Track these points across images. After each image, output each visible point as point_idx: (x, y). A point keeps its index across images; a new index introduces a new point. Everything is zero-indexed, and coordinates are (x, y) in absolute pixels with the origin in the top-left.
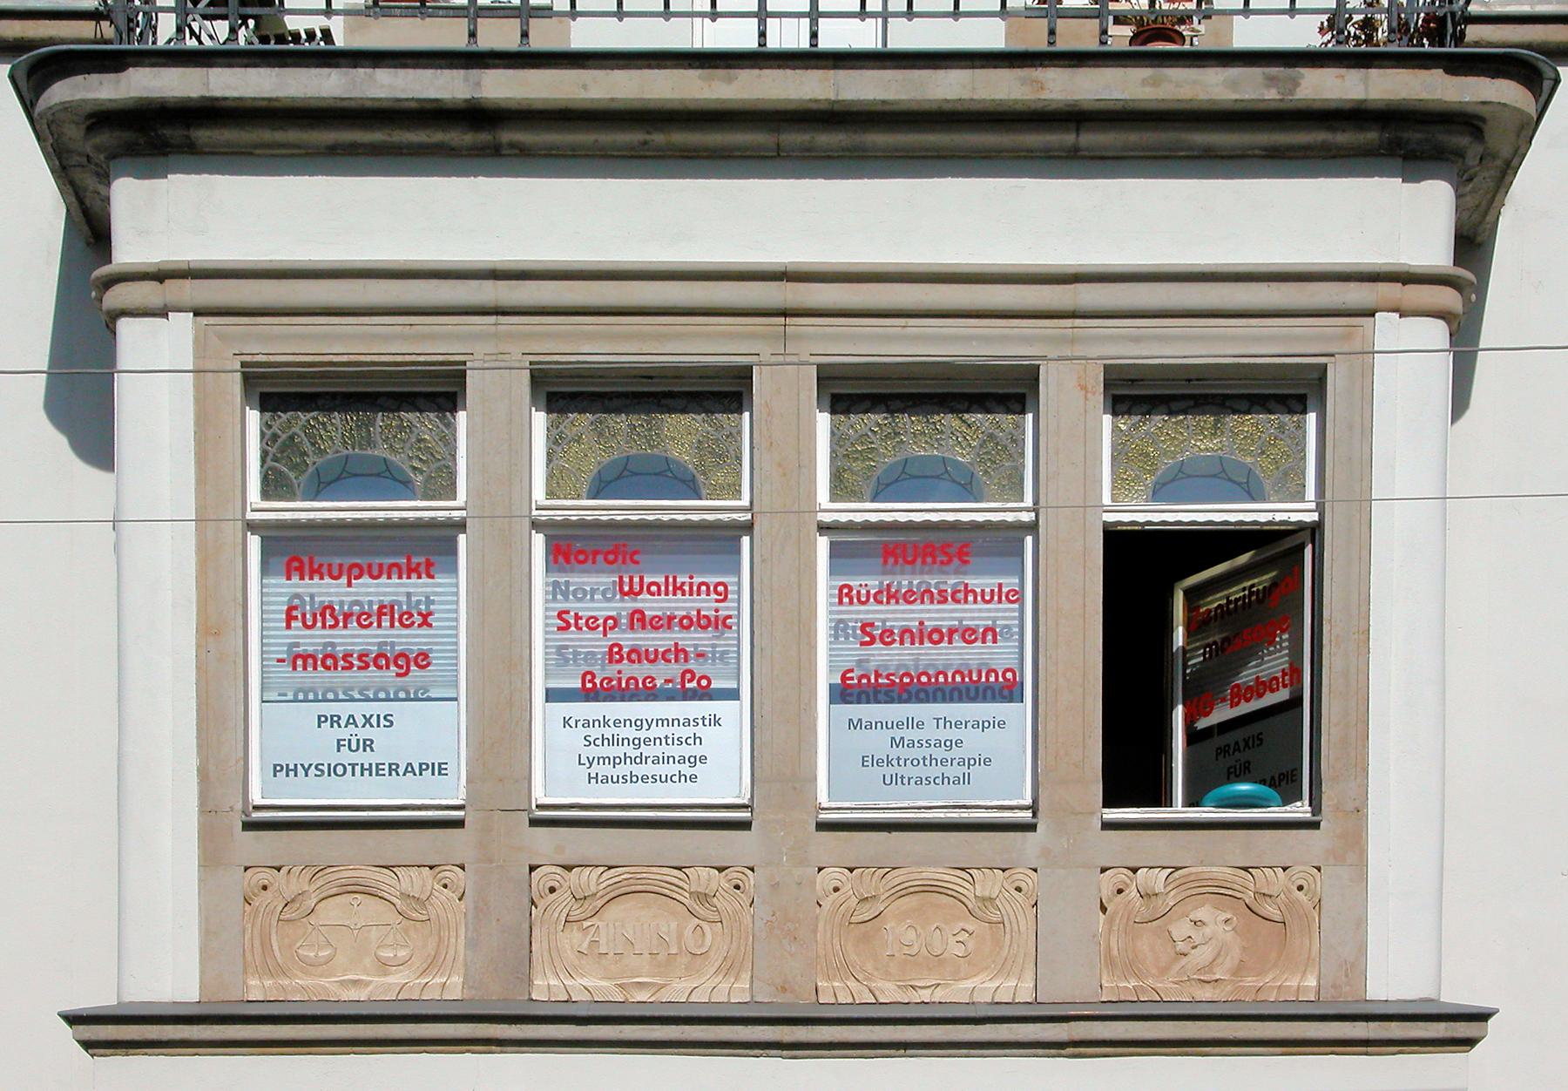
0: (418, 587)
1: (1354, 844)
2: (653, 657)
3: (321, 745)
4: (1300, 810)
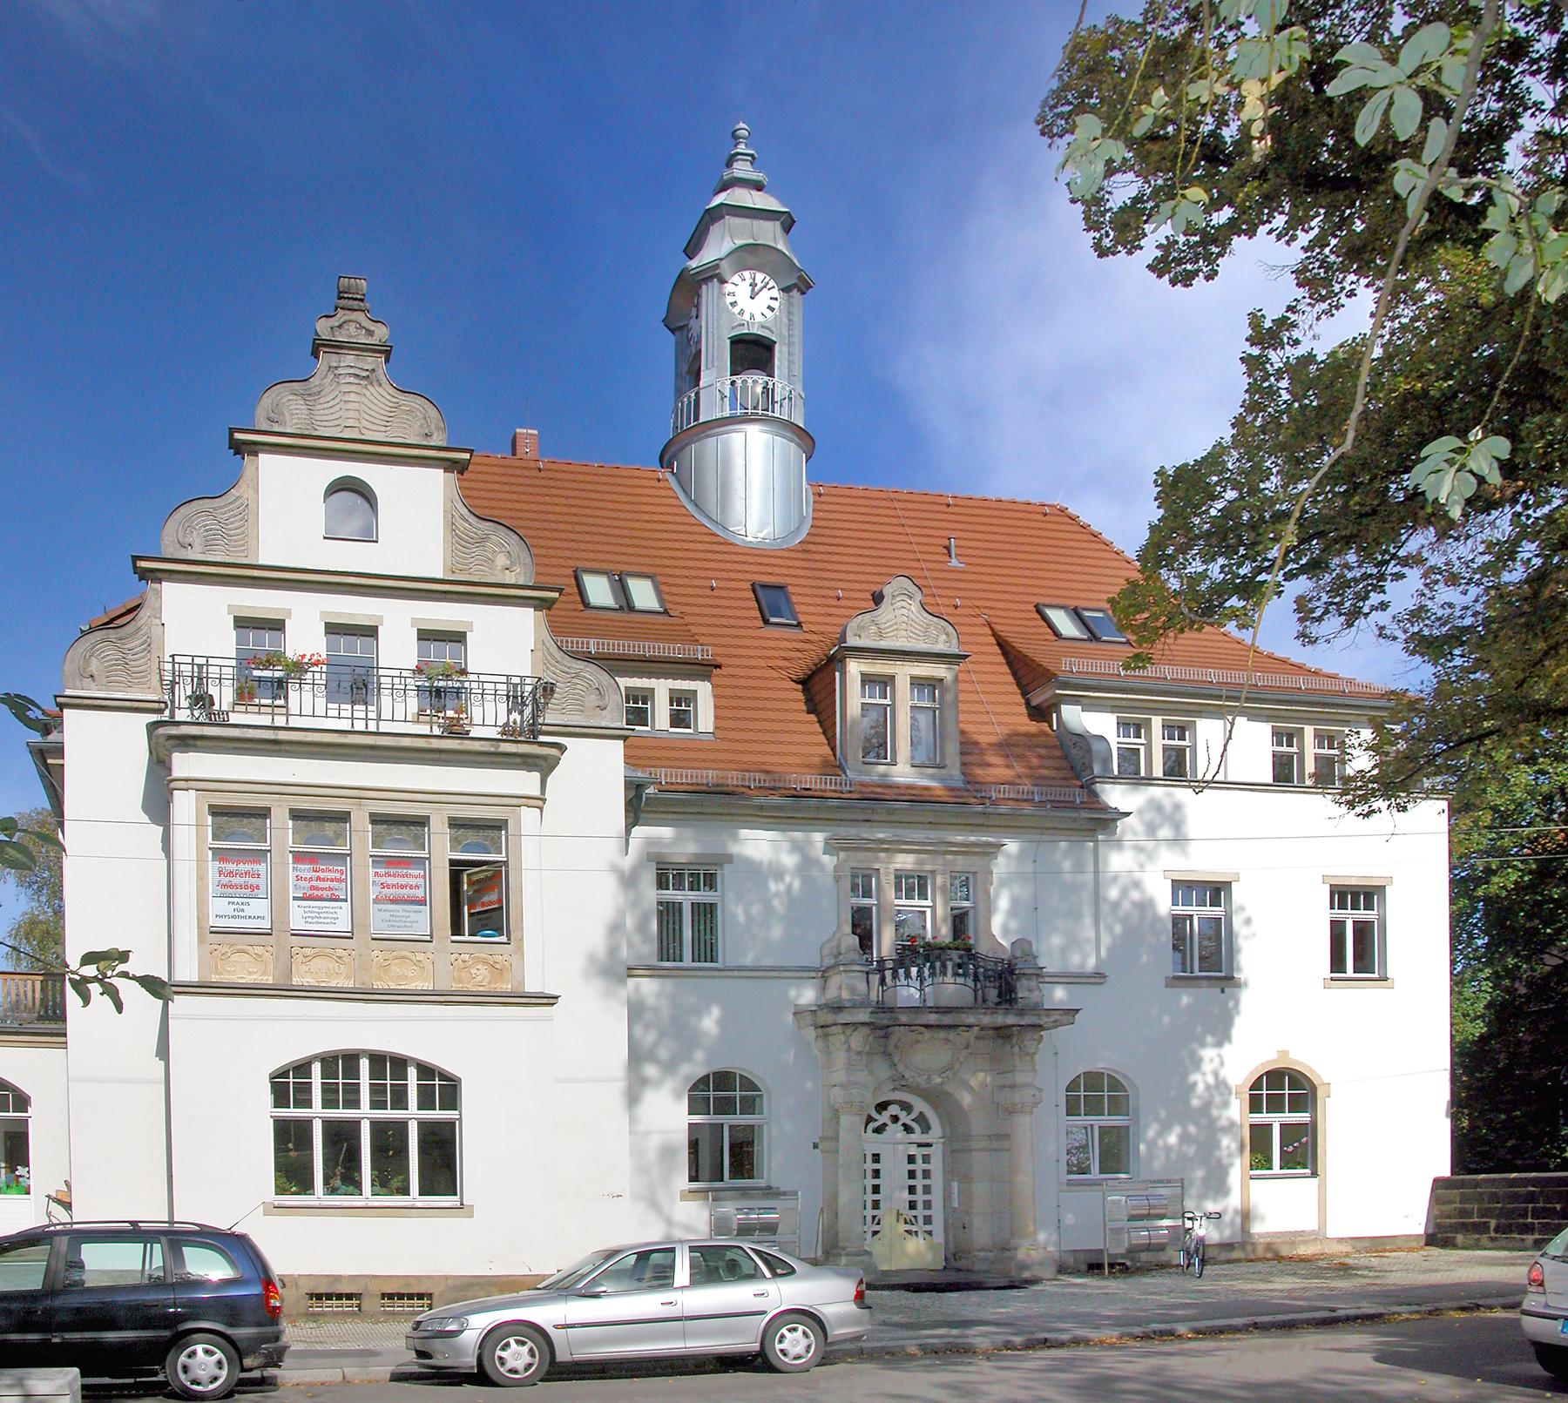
0: (256, 867)
1: (520, 949)
2: (322, 889)
3: (230, 910)
4: (503, 939)
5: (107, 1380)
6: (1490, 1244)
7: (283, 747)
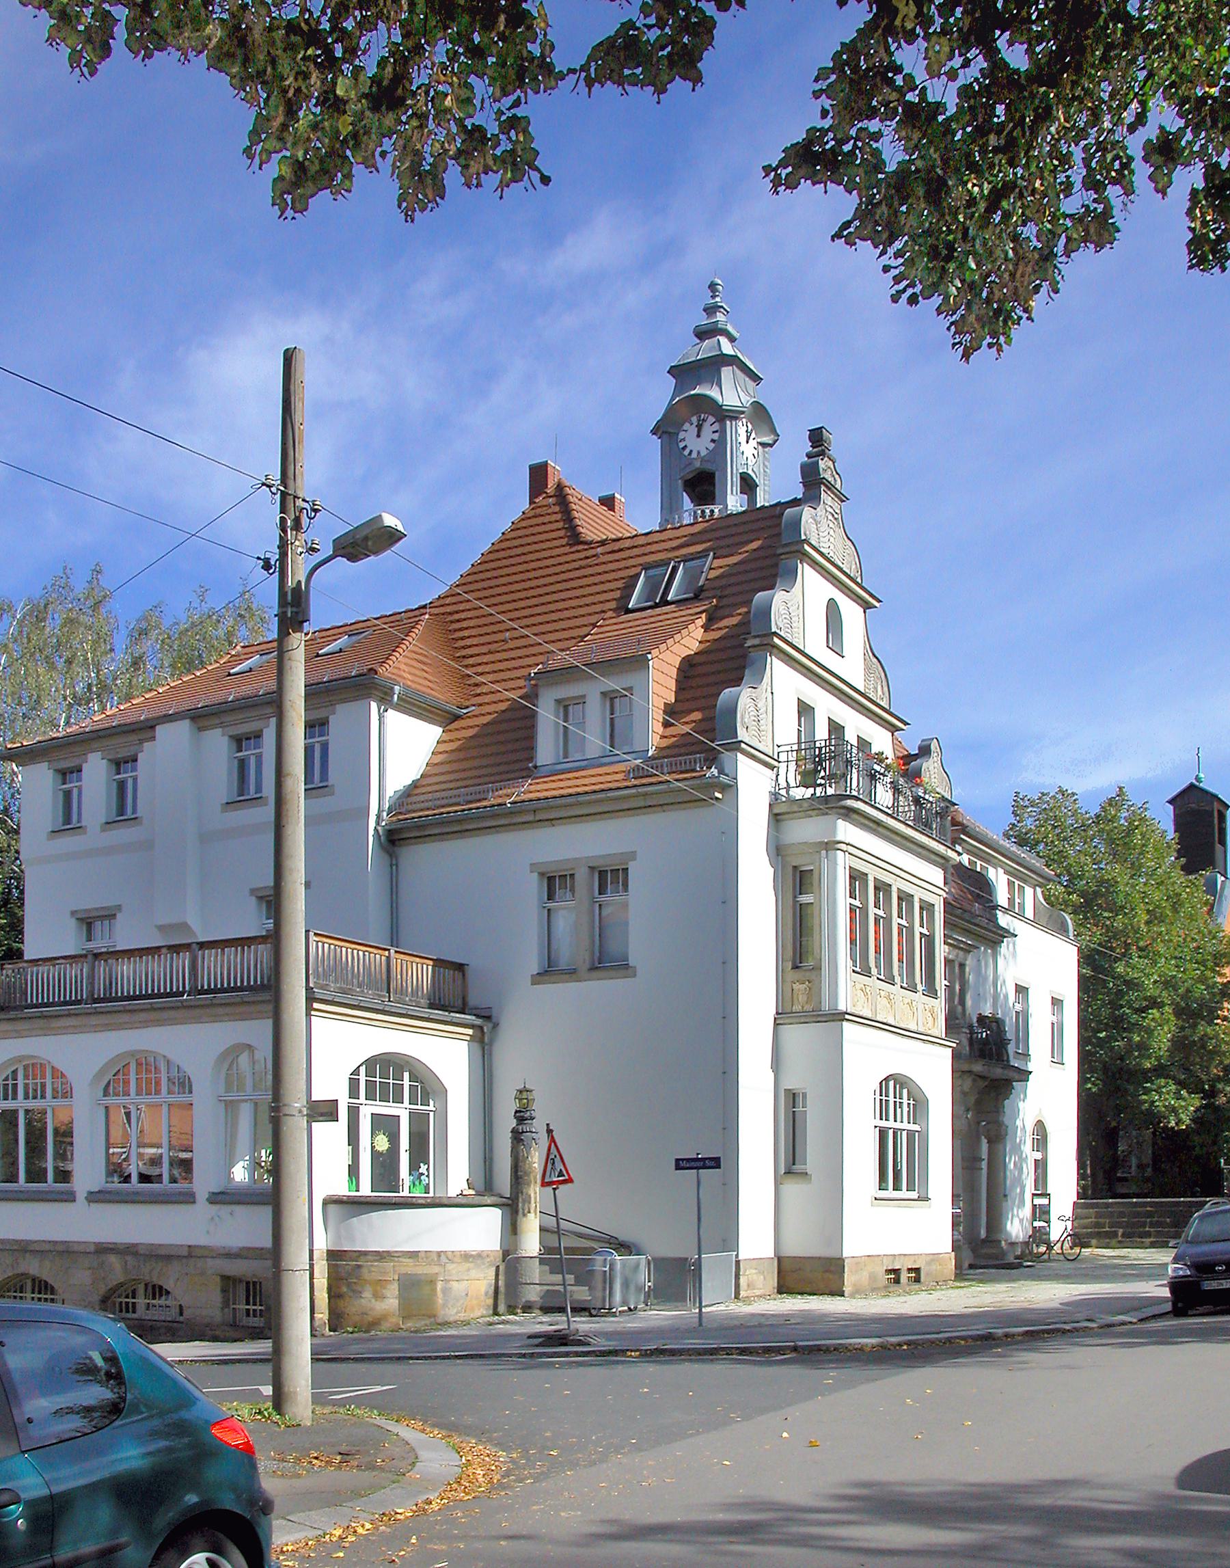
5: (379, 1388)
6: (1118, 1245)
7: (880, 829)
